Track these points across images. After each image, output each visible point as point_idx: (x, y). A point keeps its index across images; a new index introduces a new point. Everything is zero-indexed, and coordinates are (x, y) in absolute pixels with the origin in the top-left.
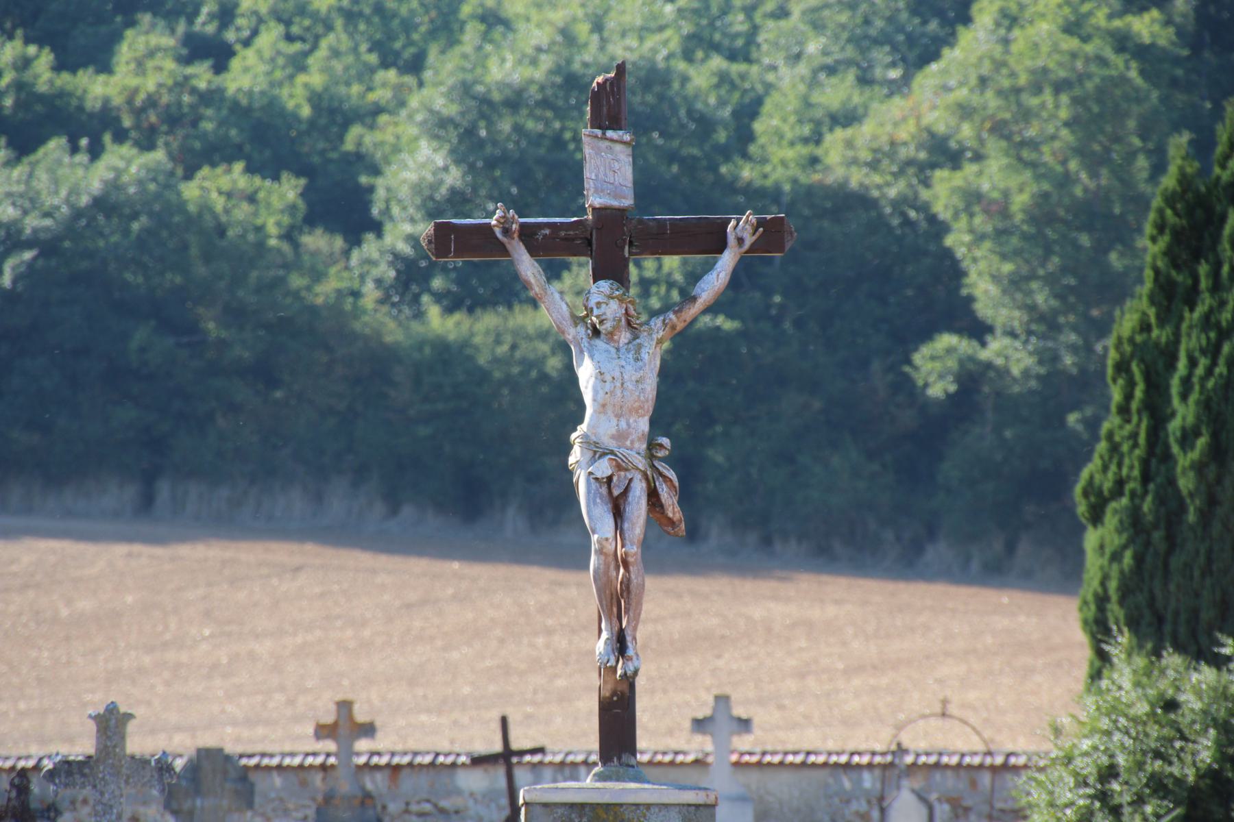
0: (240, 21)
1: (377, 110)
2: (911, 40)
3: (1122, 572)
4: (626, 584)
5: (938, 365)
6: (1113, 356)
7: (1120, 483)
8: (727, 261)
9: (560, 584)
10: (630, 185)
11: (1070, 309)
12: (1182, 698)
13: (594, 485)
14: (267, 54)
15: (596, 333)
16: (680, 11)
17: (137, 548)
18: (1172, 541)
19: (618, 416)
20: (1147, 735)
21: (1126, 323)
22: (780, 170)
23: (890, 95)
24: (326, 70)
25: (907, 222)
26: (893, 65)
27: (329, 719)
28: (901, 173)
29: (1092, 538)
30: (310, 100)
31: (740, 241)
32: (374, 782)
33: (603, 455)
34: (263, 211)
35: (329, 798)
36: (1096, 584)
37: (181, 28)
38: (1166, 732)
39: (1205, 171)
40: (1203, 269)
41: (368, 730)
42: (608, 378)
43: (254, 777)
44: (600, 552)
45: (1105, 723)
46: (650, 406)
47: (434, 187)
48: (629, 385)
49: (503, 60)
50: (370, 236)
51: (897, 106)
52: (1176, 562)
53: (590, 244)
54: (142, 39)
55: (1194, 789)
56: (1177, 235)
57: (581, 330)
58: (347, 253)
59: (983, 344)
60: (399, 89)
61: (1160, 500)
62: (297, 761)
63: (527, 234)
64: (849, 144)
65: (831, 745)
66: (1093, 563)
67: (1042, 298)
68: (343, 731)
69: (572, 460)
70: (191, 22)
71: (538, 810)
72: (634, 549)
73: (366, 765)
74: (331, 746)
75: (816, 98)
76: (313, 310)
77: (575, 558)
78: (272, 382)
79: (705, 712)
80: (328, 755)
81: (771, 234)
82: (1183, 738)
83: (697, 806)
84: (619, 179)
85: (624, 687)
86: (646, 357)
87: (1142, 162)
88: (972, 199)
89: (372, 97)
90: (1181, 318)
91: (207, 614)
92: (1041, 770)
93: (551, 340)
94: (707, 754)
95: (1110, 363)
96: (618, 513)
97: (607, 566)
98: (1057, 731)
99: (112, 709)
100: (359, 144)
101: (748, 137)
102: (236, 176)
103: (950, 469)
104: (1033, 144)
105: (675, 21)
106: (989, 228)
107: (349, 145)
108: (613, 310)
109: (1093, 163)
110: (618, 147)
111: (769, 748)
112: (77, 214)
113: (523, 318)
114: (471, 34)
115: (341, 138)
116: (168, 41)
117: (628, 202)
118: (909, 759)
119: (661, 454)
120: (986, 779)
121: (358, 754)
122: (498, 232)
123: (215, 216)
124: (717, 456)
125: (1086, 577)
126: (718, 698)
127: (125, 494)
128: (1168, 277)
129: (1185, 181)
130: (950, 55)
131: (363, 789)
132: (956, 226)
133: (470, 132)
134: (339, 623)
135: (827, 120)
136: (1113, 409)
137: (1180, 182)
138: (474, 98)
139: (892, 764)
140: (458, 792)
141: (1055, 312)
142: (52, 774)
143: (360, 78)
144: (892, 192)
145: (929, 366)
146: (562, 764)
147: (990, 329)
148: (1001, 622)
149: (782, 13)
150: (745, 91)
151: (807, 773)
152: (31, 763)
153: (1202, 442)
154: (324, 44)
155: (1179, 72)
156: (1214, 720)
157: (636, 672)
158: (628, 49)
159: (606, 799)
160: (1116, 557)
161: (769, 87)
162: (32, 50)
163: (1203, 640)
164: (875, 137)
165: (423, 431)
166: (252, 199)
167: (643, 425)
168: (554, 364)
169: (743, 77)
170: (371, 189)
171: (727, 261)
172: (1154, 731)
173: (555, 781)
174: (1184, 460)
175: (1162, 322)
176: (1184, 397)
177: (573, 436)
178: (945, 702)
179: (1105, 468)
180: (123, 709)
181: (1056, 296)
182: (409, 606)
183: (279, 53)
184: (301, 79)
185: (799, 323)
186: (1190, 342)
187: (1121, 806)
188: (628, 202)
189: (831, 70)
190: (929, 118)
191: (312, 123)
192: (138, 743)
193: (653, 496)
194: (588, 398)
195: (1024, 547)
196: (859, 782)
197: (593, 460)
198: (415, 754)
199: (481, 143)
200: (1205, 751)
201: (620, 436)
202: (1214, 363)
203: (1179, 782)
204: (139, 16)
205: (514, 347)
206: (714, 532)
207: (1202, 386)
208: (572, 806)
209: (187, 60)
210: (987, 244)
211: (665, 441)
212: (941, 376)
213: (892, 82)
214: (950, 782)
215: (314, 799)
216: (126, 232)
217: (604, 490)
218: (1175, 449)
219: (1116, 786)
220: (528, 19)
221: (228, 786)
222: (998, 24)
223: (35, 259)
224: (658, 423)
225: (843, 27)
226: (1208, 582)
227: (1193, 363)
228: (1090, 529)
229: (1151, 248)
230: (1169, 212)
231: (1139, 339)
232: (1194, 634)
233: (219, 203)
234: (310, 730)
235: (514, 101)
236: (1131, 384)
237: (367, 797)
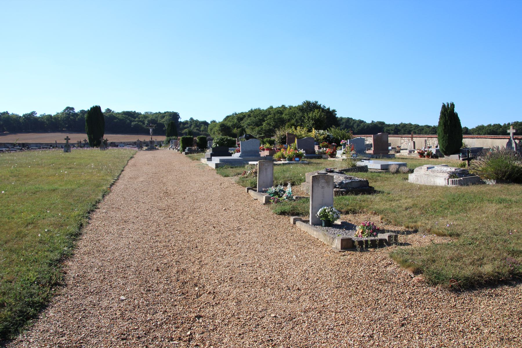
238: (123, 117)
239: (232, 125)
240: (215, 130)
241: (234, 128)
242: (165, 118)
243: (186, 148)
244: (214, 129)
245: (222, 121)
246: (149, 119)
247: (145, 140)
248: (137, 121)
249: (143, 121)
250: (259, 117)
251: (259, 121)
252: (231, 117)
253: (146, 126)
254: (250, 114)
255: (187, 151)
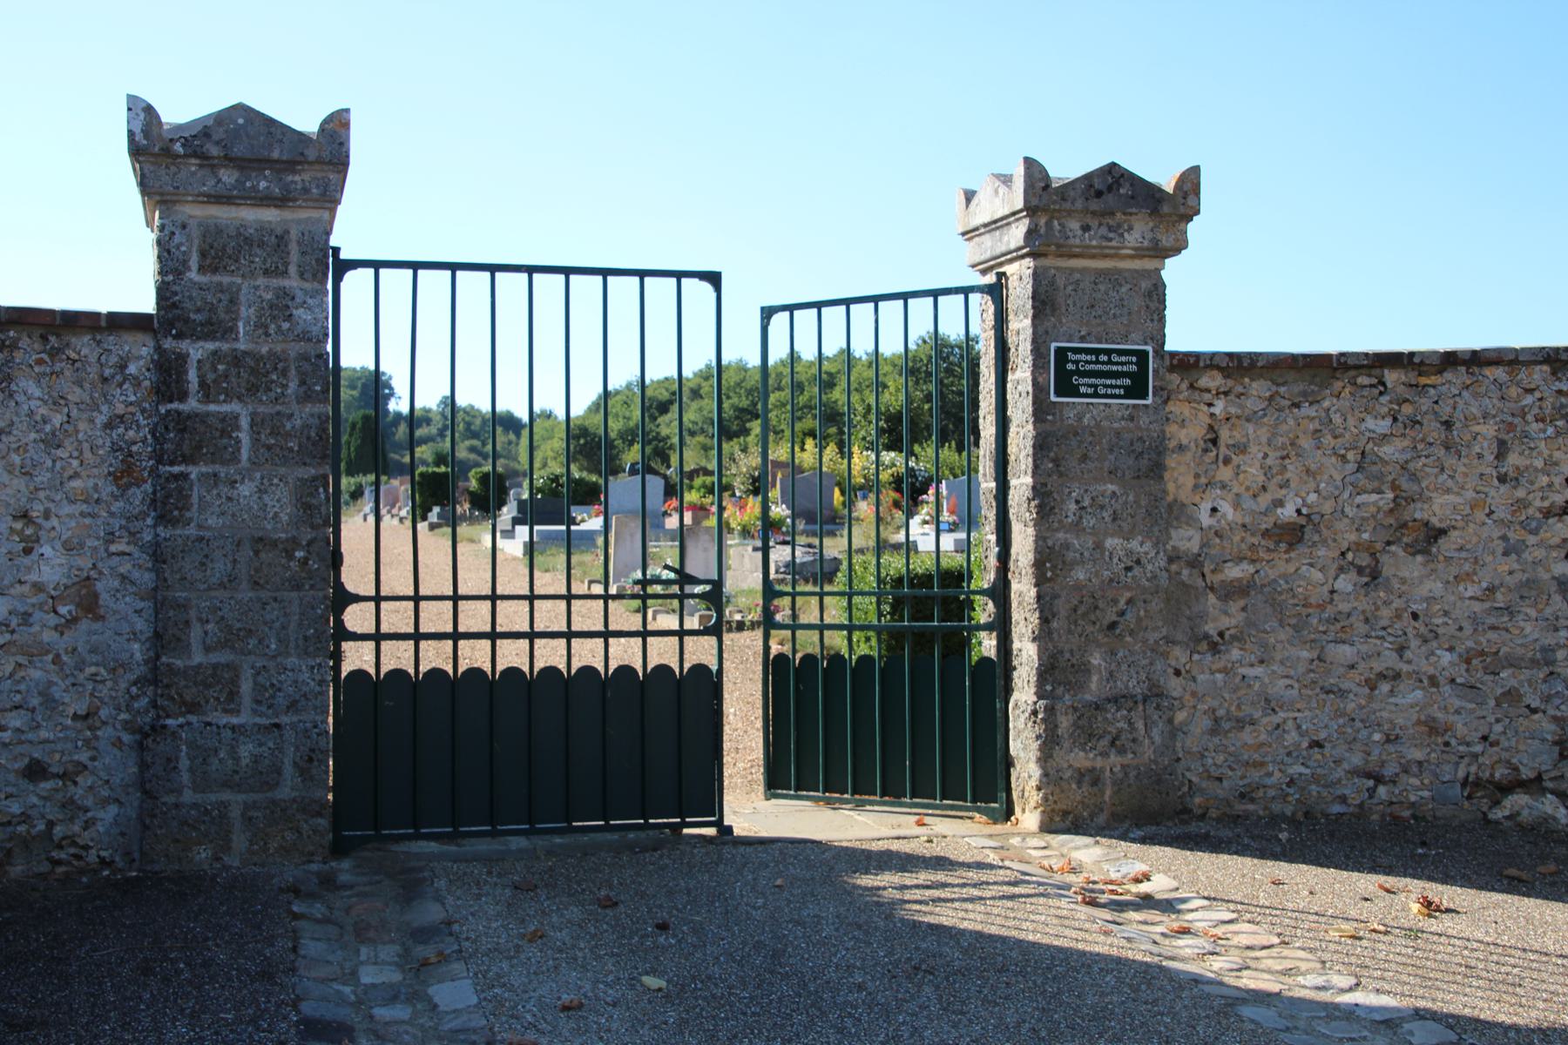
239: (619, 431)
240: (550, 454)
241: (631, 443)
243: (431, 510)
244: (542, 447)
245: (350, 629)
250: (735, 400)
251: (737, 418)
252: (618, 398)
254: (700, 387)
255: (435, 520)
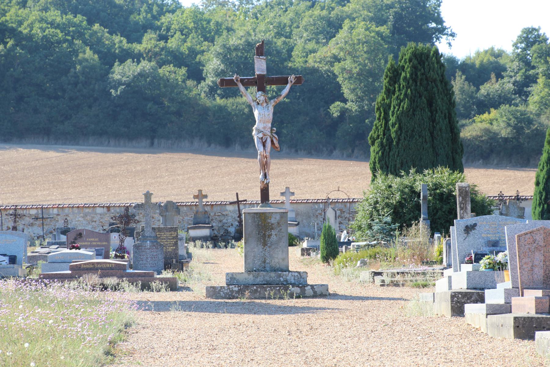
0: (171, 31)
1: (203, 51)
2: (328, 33)
3: (379, 156)
4: (266, 162)
5: (336, 109)
6: (376, 106)
7: (378, 136)
8: (288, 86)
9: (249, 162)
10: (265, 69)
11: (366, 95)
12: (393, 185)
13: (259, 139)
14: (177, 39)
15: (258, 104)
16: (274, 27)
17: (150, 155)
18: (390, 149)
19: (264, 123)
20: (385, 194)
21: (379, 99)
22: (298, 64)
23: (324, 46)
24: (191, 42)
25: (328, 76)
26: (324, 39)
27: (197, 194)
28: (327, 64)
29: (372, 149)
30: (188, 49)
31: (291, 82)
32: (207, 208)
33: (261, 132)
34: (177, 75)
35: (197, 212)
36: (373, 159)
37: (158, 32)
38: (390, 193)
39: (396, 63)
40: (397, 86)
41: (206, 196)
42: (261, 114)
43: (180, 207)
44: (260, 155)
45: (375, 191)
46: (271, 121)
47: (217, 69)
48: (266, 116)
49: (233, 39)
50: (203, 81)
51: (325, 49)
52: (391, 154)
53: (256, 83)
54: (148, 35)
55: (395, 205)
56: (390, 78)
57: (255, 103)
58: (197, 85)
59: (346, 104)
60: (209, 46)
61: (387, 140)
62: (189, 204)
63: (242, 81)
64: (314, 57)
65: (312, 198)
66: (372, 155)
67: (360, 93)
68: (200, 197)
69: (253, 133)
70: (160, 32)
71: (247, 214)
72: (268, 154)
73: (205, 204)
74: (197, 200)
75: (306, 47)
76: (190, 99)
77: (254, 155)
78: (181, 116)
79: (284, 191)
80: (197, 202)
81: (298, 80)
82: (393, 194)
83: (284, 213)
84: (263, 68)
85: (266, 186)
86: (270, 109)
87: (382, 61)
88: (343, 69)
89: (202, 48)
90: (392, 97)
91: (167, 170)
92: (361, 202)
93: (245, 104)
94: (284, 201)
95: (376, 108)
96: (264, 146)
97: (262, 158)
98: (365, 193)
99: (148, 192)
100: (200, 59)
101: (290, 56)
102: (171, 68)
103: (339, 133)
104: (358, 57)
105: (273, 29)
106: (347, 77)
107: (197, 60)
108: (262, 98)
109: (372, 61)
110: (263, 60)
111: (298, 199)
112: (135, 77)
113: (239, 100)
114: (225, 33)
115: (196, 58)
116: (154, 36)
117: (265, 73)
118: (331, 201)
119: (274, 132)
120: (348, 205)
121: (204, 202)
122: (235, 81)
123: (167, 77)
124: (285, 131)
125: (371, 158)
126: (286, 188)
127: (146, 142)
128: (389, 88)
129: (392, 66)
130: (338, 36)
131: (205, 210)
132: (339, 76)
133: (226, 56)
134: (197, 172)
135: (309, 52)
136: (377, 119)
137: (391, 66)
138: (227, 48)
139: (327, 202)
140: (227, 210)
141: (363, 96)
142: (135, 207)
143: (199, 44)
144: (324, 69)
145: (334, 109)
146: (251, 203)
147: (347, 100)
148: (350, 169)
149: (298, 27)
150: (290, 45)
151: (307, 205)
152: (128, 205)
153: (397, 126)
154: (190, 36)
155: (390, 40)
156: (400, 190)
157: (269, 182)
158: (262, 36)
159: (262, 211)
160: (377, 153)
161: (295, 44)
162: (122, 38)
163: (397, 171)
164: (320, 56)
165: (216, 127)
166: (175, 73)
167: (270, 125)
168: (246, 110)
169: (289, 42)
170: (203, 70)
171: (288, 86)
172: (386, 192)
173: (249, 208)
174: (393, 130)
175: (387, 99)
176: (393, 116)
177: (253, 128)
178: (339, 187)
179: (375, 133)
180: (150, 192)
181: (363, 93)
182: (213, 168)
183: (180, 38)
184: (185, 44)
185: (303, 100)
186: (394, 103)
187: (379, 210)
188: (265, 73)
189: (309, 40)
190: (334, 51)
191: (188, 54)
192: (154, 200)
193: (272, 141)
194: (257, 119)
195: (356, 151)
196: (320, 206)
197: (258, 134)
198: (217, 202)
199: (228, 59)
200: (398, 197)
201: (264, 128)
202: (399, 108)
203: (392, 204)
204: (148, 30)
205: (237, 106)
206: (284, 149)
207: (397, 113)
208: (255, 213)
209: (159, 40)
210: (347, 81)
211: (275, 129)
212: (336, 112)
213: (324, 42)
214: (340, 206)
215: (193, 212)
216: (146, 81)
217: (261, 140)
218: (391, 128)
219: (378, 205)
220: (238, 29)
221: (174, 210)
222: (349, 29)
223: (125, 88)
224: (273, 125)
225: (312, 30)
226: (398, 158)
227: (394, 108)
228: (372, 146)
229: (385, 81)
230: (388, 73)
231: (382, 102)
232: (395, 170)
233: (167, 74)
234: (192, 197)
235: (236, 49)
236: (381, 113)
237: (206, 212)
238: (52, 24)
242: (342, 34)
246: (233, 41)
247: (200, 196)
248: (150, 55)
249: (193, 53)
253: (212, 91)
